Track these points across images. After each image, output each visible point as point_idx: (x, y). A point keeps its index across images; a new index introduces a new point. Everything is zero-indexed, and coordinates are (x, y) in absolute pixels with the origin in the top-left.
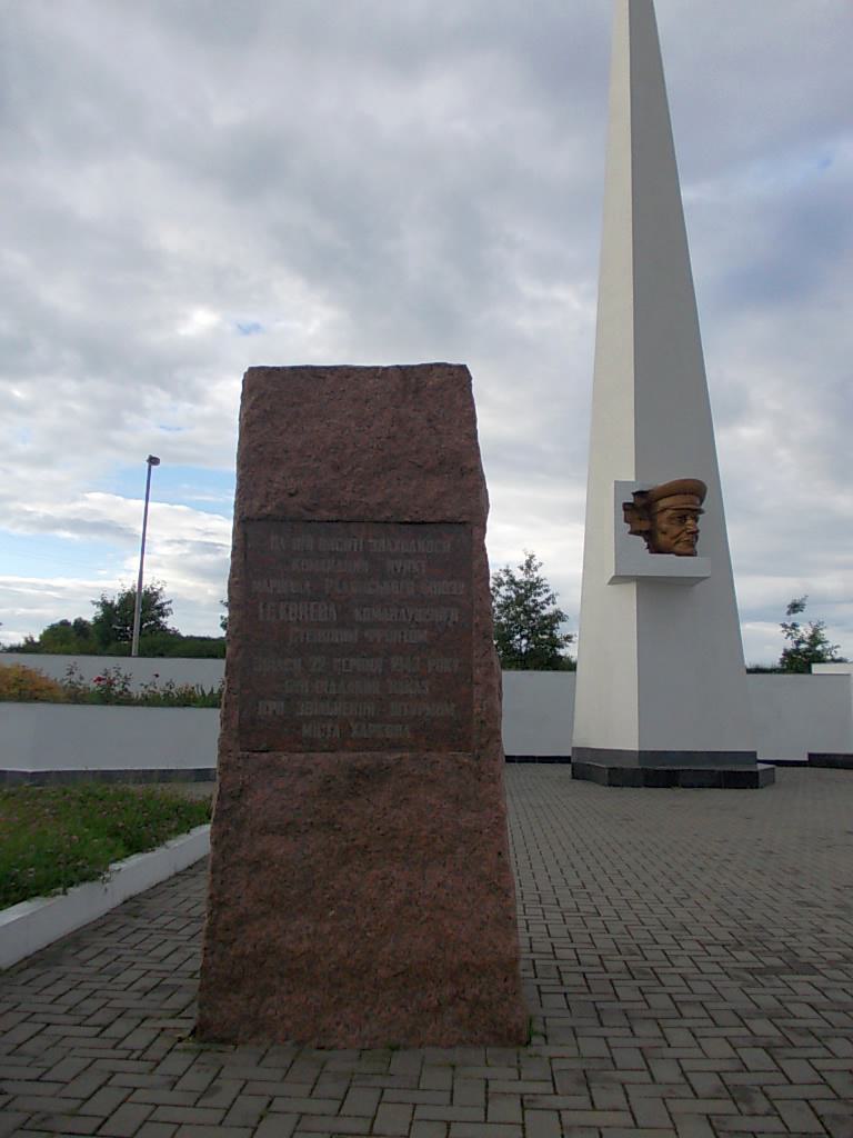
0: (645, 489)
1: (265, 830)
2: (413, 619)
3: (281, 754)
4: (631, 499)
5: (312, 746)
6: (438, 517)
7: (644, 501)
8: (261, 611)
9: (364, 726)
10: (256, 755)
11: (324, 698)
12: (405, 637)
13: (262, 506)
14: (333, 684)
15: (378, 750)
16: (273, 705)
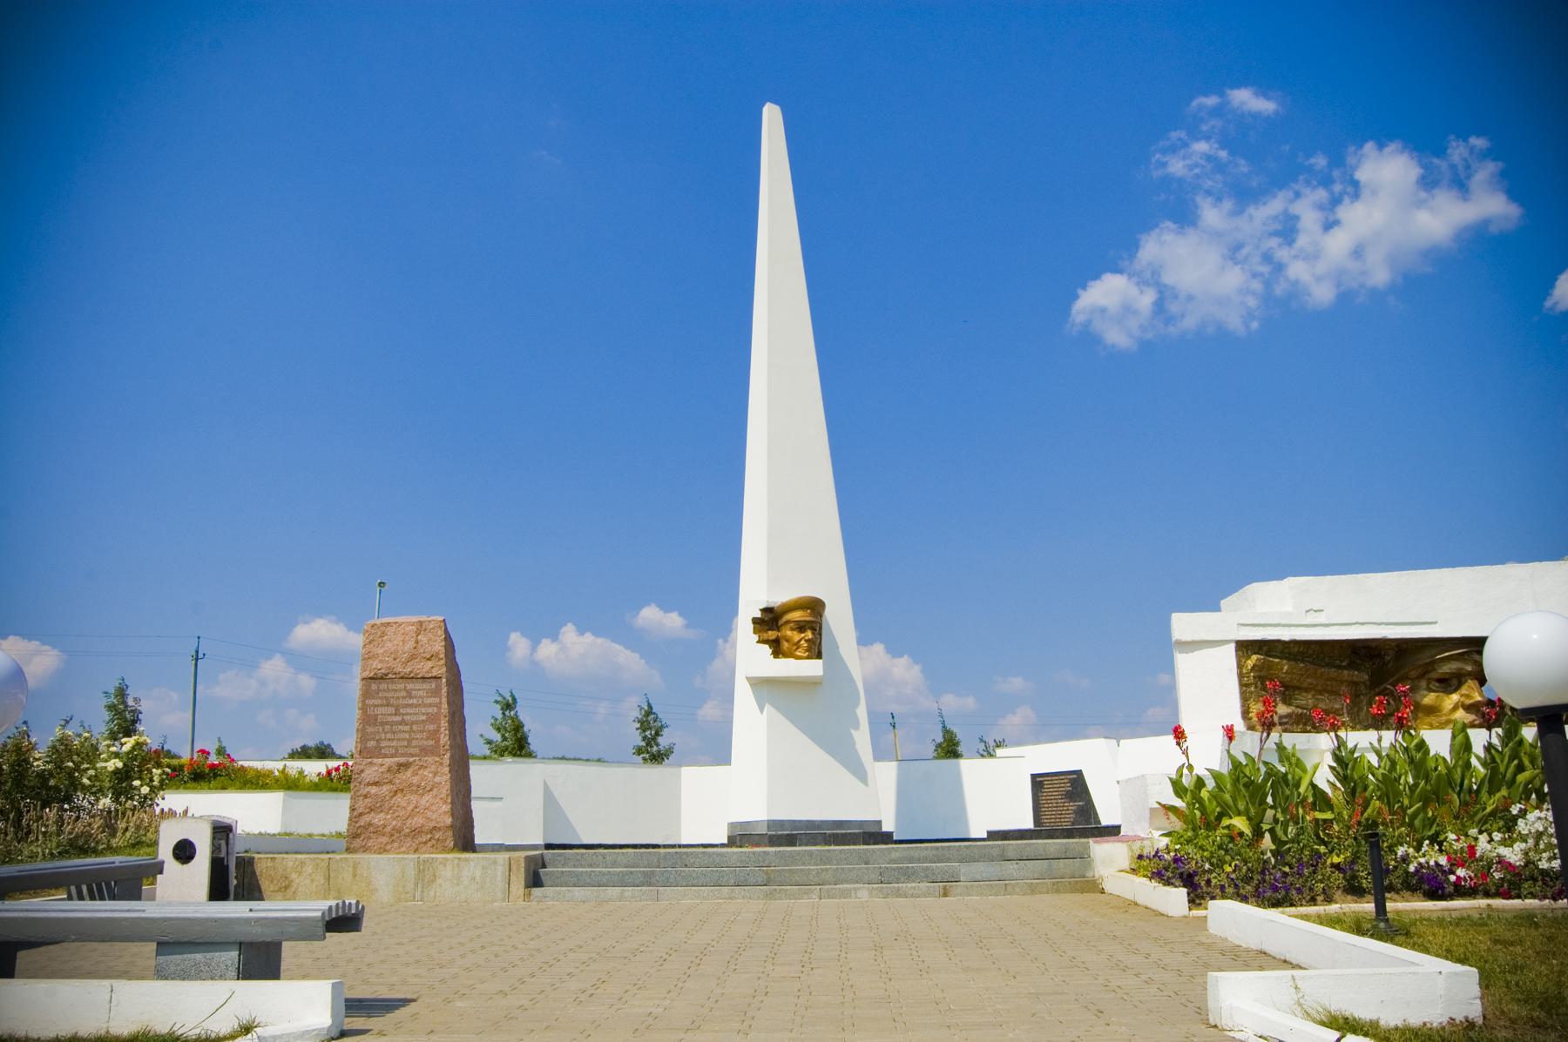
1: (369, 784)
4: (759, 615)
5: (385, 756)
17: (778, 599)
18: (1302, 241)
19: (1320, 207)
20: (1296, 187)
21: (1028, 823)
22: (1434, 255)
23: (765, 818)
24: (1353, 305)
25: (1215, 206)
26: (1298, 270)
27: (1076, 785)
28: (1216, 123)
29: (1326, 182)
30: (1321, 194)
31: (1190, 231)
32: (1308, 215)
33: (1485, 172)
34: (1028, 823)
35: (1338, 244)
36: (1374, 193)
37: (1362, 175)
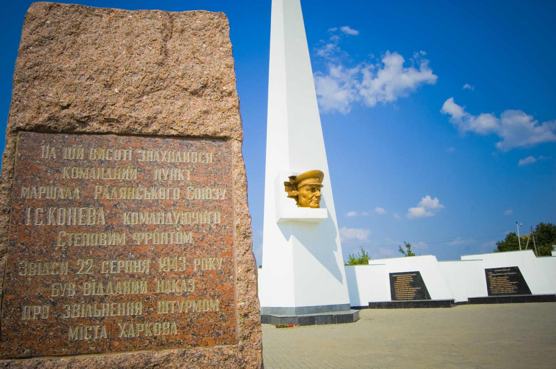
0: (295, 175)
2: (179, 222)
3: (45, 359)
4: (288, 180)
6: (201, 131)
7: (294, 181)
8: (29, 216)
9: (132, 326)
10: (17, 362)
11: (91, 299)
12: (160, 327)
13: (33, 118)
14: (101, 286)
15: (146, 348)
16: (38, 309)
17: (299, 172)
18: (365, 83)
19: (370, 70)
20: (364, 63)
21: (388, 298)
22: (407, 90)
23: (294, 307)
24: (381, 108)
25: (336, 68)
26: (363, 92)
27: (416, 279)
28: (337, 37)
29: (374, 62)
30: (372, 66)
31: (327, 76)
32: (367, 73)
33: (424, 64)
34: (388, 298)
35: (377, 84)
36: (388, 67)
37: (385, 61)
